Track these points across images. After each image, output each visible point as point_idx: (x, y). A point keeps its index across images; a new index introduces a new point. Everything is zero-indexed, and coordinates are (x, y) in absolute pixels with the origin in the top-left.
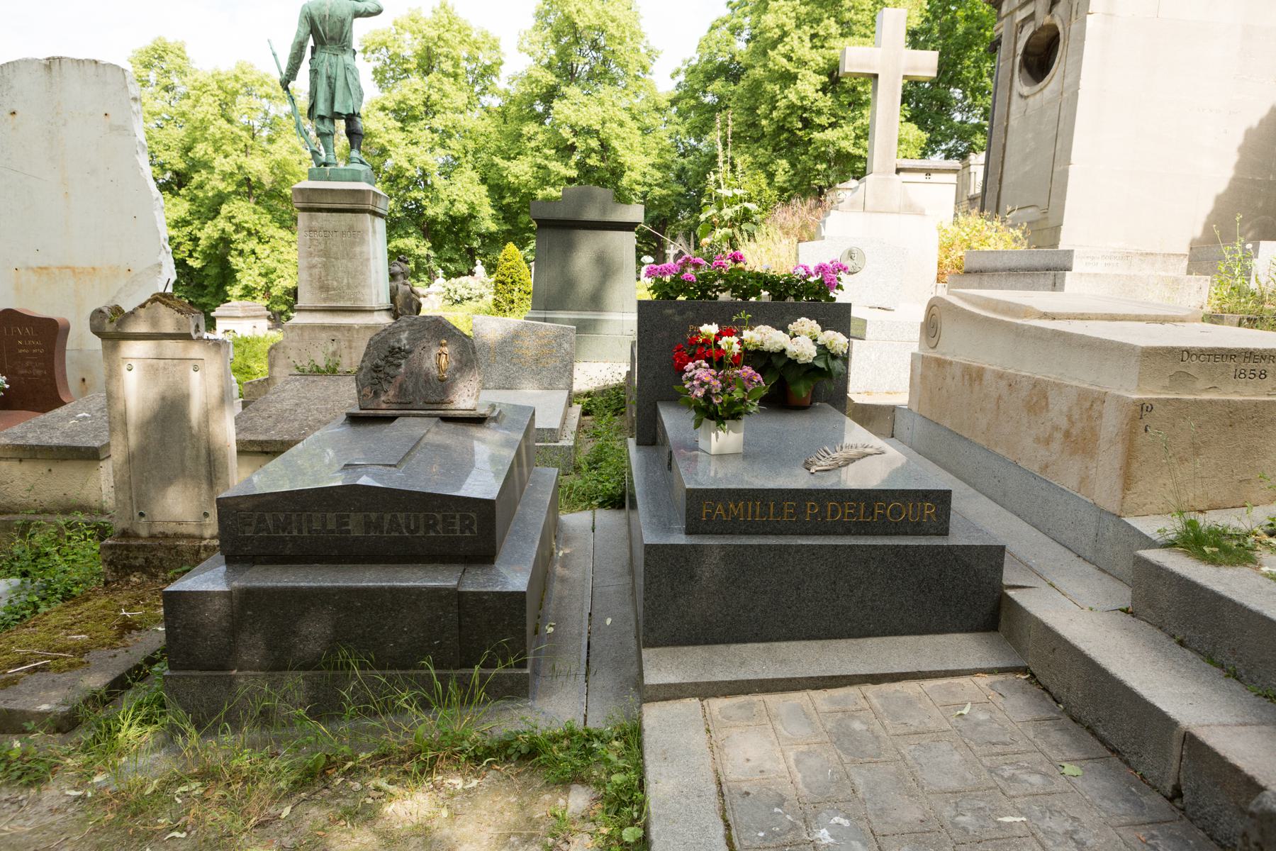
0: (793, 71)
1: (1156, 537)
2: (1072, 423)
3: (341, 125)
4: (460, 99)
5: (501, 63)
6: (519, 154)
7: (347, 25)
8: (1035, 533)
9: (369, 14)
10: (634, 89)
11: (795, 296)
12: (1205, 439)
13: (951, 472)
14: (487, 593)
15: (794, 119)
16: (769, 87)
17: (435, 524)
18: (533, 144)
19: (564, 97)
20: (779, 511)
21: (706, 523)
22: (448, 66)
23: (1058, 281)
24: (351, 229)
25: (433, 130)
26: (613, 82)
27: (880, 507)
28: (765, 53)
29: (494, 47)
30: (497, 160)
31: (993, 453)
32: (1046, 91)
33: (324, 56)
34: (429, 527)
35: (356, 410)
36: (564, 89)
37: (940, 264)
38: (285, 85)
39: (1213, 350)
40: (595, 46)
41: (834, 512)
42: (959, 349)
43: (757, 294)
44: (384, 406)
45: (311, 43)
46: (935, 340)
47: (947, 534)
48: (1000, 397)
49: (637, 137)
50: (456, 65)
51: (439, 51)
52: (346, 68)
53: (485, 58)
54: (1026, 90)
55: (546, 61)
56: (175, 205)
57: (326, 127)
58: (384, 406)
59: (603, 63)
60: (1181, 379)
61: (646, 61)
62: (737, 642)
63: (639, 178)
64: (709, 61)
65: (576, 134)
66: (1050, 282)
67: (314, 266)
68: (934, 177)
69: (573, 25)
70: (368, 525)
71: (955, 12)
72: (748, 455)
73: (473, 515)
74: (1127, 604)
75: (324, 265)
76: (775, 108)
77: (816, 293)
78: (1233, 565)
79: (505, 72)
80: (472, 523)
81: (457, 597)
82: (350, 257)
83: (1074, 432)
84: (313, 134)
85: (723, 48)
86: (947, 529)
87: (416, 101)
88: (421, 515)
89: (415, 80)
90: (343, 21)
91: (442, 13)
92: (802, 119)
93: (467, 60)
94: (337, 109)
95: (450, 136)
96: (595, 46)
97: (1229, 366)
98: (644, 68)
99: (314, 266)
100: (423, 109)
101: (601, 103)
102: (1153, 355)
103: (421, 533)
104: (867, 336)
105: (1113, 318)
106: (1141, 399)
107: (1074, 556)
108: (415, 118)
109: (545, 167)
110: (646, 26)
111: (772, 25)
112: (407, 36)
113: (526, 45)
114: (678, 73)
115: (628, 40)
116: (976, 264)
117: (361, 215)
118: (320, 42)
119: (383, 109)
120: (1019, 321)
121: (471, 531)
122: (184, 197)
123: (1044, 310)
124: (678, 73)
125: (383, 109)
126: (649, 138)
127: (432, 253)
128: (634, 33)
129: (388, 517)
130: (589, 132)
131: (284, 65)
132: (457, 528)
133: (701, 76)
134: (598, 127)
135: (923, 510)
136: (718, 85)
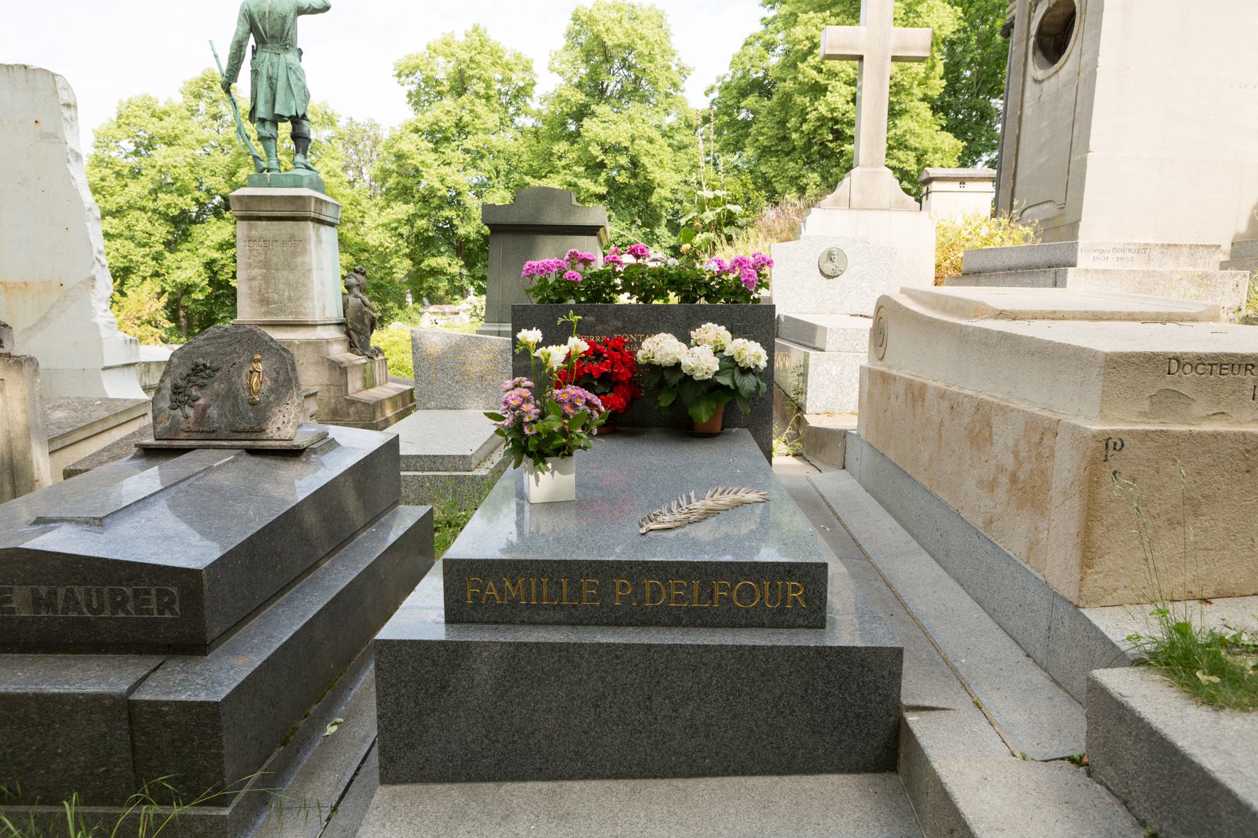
0: (822, 82)
1: (1124, 647)
2: (1019, 463)
3: (285, 129)
4: (492, 120)
5: (534, 84)
6: (550, 172)
7: (289, 21)
8: (978, 614)
9: (314, 11)
10: (665, 106)
11: (707, 297)
12: (1208, 492)
13: (895, 517)
14: (167, 703)
15: (824, 130)
16: (799, 99)
17: (125, 600)
18: (563, 162)
19: (593, 114)
20: (576, 593)
21: (473, 607)
22: (480, 87)
23: (1059, 280)
24: (292, 237)
25: (467, 151)
26: (644, 99)
27: (723, 588)
28: (795, 66)
29: (527, 69)
30: (528, 179)
31: (934, 497)
32: (1061, 73)
33: (265, 56)
34: (116, 606)
35: (150, 441)
36: (593, 107)
37: (938, 266)
38: (227, 88)
39: (1217, 356)
40: (626, 64)
41: (656, 593)
42: (907, 364)
43: (664, 295)
44: (183, 435)
45: (252, 41)
46: (882, 349)
47: (822, 626)
48: (941, 424)
49: (667, 155)
50: (488, 87)
51: (471, 73)
52: (289, 68)
53: (518, 79)
54: (1040, 74)
55: (576, 80)
56: (219, 228)
57: (267, 130)
58: (183, 435)
59: (635, 82)
60: (1167, 400)
61: (677, 78)
62: (513, 780)
63: (669, 195)
64: (743, 77)
65: (605, 151)
66: (1051, 281)
67: (254, 279)
68: (969, 186)
69: (603, 45)
70: (37, 602)
71: (994, 22)
72: (582, 504)
73: (174, 590)
74: (1078, 749)
75: (265, 277)
76: (805, 120)
77: (733, 294)
78: (1243, 708)
79: (538, 91)
80: (172, 601)
81: (127, 709)
82: (292, 268)
83: (1021, 476)
84: (254, 136)
85: (756, 62)
86: (824, 619)
87: (447, 122)
88: (106, 590)
89: (448, 102)
90: (284, 18)
91: (474, 36)
92: (833, 131)
93: (502, 81)
94: (277, 111)
95: (482, 157)
96: (626, 64)
97: (1243, 382)
98: (674, 85)
99: (254, 279)
100: (454, 131)
101: (631, 120)
102: (1120, 364)
103: (107, 613)
104: (828, 347)
105: (1096, 317)
106: (1104, 432)
107: (1020, 655)
108: (447, 139)
109: (575, 185)
110: (676, 43)
111: (802, 37)
112: (441, 59)
113: (557, 65)
114: (712, 90)
115: (658, 57)
116: (975, 265)
117: (302, 223)
118: (261, 41)
119: (417, 130)
120: (964, 322)
121: (172, 611)
122: (228, 220)
123: (1000, 308)
124: (712, 90)
125: (417, 130)
126: (681, 155)
127: (465, 272)
128: (664, 51)
129: (62, 591)
130: (617, 149)
131: (225, 65)
132: (153, 606)
133: (735, 92)
134: (627, 144)
135: (785, 592)
136: (751, 101)
